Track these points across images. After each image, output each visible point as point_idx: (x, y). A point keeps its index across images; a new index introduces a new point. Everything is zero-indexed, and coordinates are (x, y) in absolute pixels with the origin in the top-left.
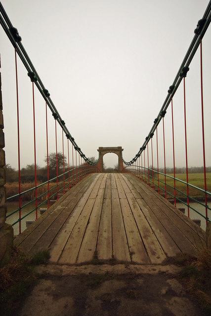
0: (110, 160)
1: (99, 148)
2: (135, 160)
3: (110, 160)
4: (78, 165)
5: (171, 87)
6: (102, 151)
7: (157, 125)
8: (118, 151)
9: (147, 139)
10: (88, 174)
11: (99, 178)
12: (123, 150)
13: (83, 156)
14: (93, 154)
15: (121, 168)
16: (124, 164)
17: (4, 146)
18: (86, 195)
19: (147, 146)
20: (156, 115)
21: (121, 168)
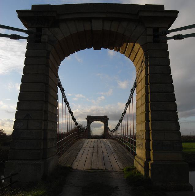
0: (97, 129)
1: (87, 116)
2: (116, 128)
3: (97, 129)
4: (66, 131)
5: (131, 89)
6: (90, 119)
7: (127, 108)
8: (104, 119)
9: (127, 105)
10: (77, 139)
11: (88, 143)
12: (108, 119)
13: (74, 119)
14: (82, 121)
15: (107, 134)
16: (109, 132)
17: (20, 93)
18: (82, 151)
19: (132, 100)
20: (127, 101)
21: (107, 134)
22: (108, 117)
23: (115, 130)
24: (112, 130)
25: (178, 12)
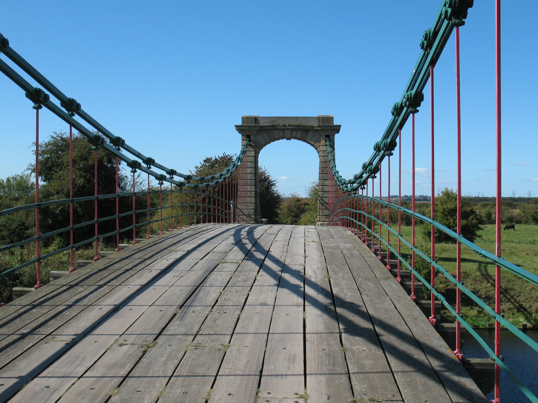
12: (337, 129)
22: (336, 123)
23: (365, 182)
24: (351, 183)
25: (340, 126)
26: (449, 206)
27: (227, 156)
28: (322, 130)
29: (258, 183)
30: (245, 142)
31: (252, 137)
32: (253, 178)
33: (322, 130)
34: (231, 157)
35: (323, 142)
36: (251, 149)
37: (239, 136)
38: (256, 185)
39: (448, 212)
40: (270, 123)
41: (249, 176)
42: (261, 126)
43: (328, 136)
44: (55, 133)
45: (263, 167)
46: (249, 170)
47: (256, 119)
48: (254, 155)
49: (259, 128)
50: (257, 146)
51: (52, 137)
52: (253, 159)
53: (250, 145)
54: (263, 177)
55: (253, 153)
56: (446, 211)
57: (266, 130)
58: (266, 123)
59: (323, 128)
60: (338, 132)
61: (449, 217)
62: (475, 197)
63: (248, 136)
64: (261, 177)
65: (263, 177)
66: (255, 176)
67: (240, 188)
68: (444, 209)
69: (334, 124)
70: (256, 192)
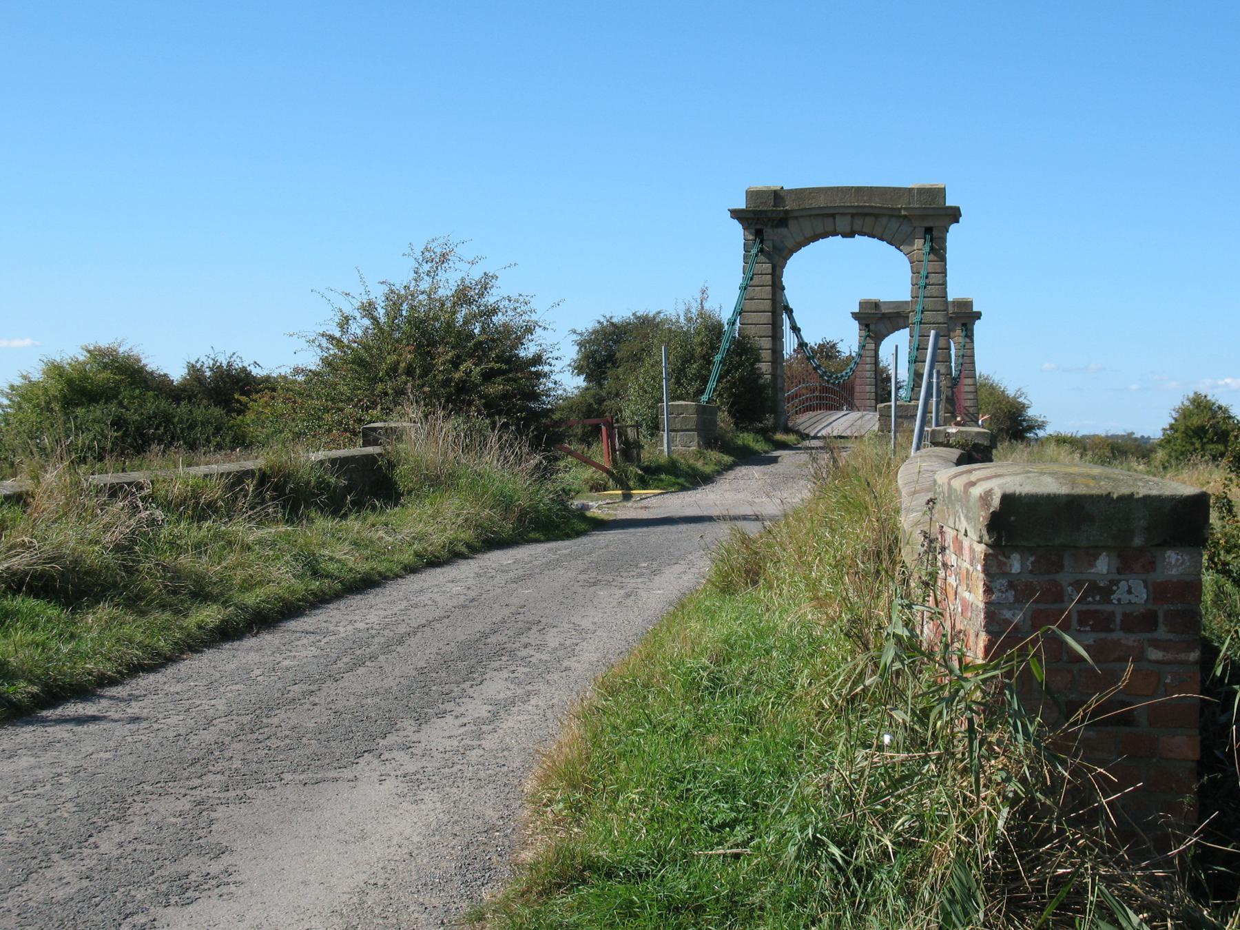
12: (954, 215)
22: (975, 309)
26: (1194, 422)
27: (828, 343)
28: (958, 318)
29: (879, 382)
30: (864, 333)
31: (872, 327)
32: (873, 376)
33: (958, 318)
34: (834, 345)
35: (918, 243)
36: (871, 341)
37: (856, 324)
38: (876, 385)
39: (1193, 431)
40: (894, 308)
41: (868, 374)
42: (883, 314)
43: (929, 230)
44: (604, 317)
45: (884, 360)
46: (868, 367)
47: (876, 305)
48: (874, 348)
49: (879, 316)
50: (878, 339)
51: (599, 322)
52: (872, 353)
53: (868, 336)
54: (885, 375)
55: (873, 346)
56: (1191, 429)
57: (889, 318)
58: (890, 309)
59: (959, 315)
60: (979, 318)
61: (1194, 440)
62: (152, 373)
63: (867, 326)
64: (881, 375)
65: (885, 375)
66: (876, 374)
67: (857, 389)
68: (1187, 426)
69: (947, 205)
70: (876, 393)
